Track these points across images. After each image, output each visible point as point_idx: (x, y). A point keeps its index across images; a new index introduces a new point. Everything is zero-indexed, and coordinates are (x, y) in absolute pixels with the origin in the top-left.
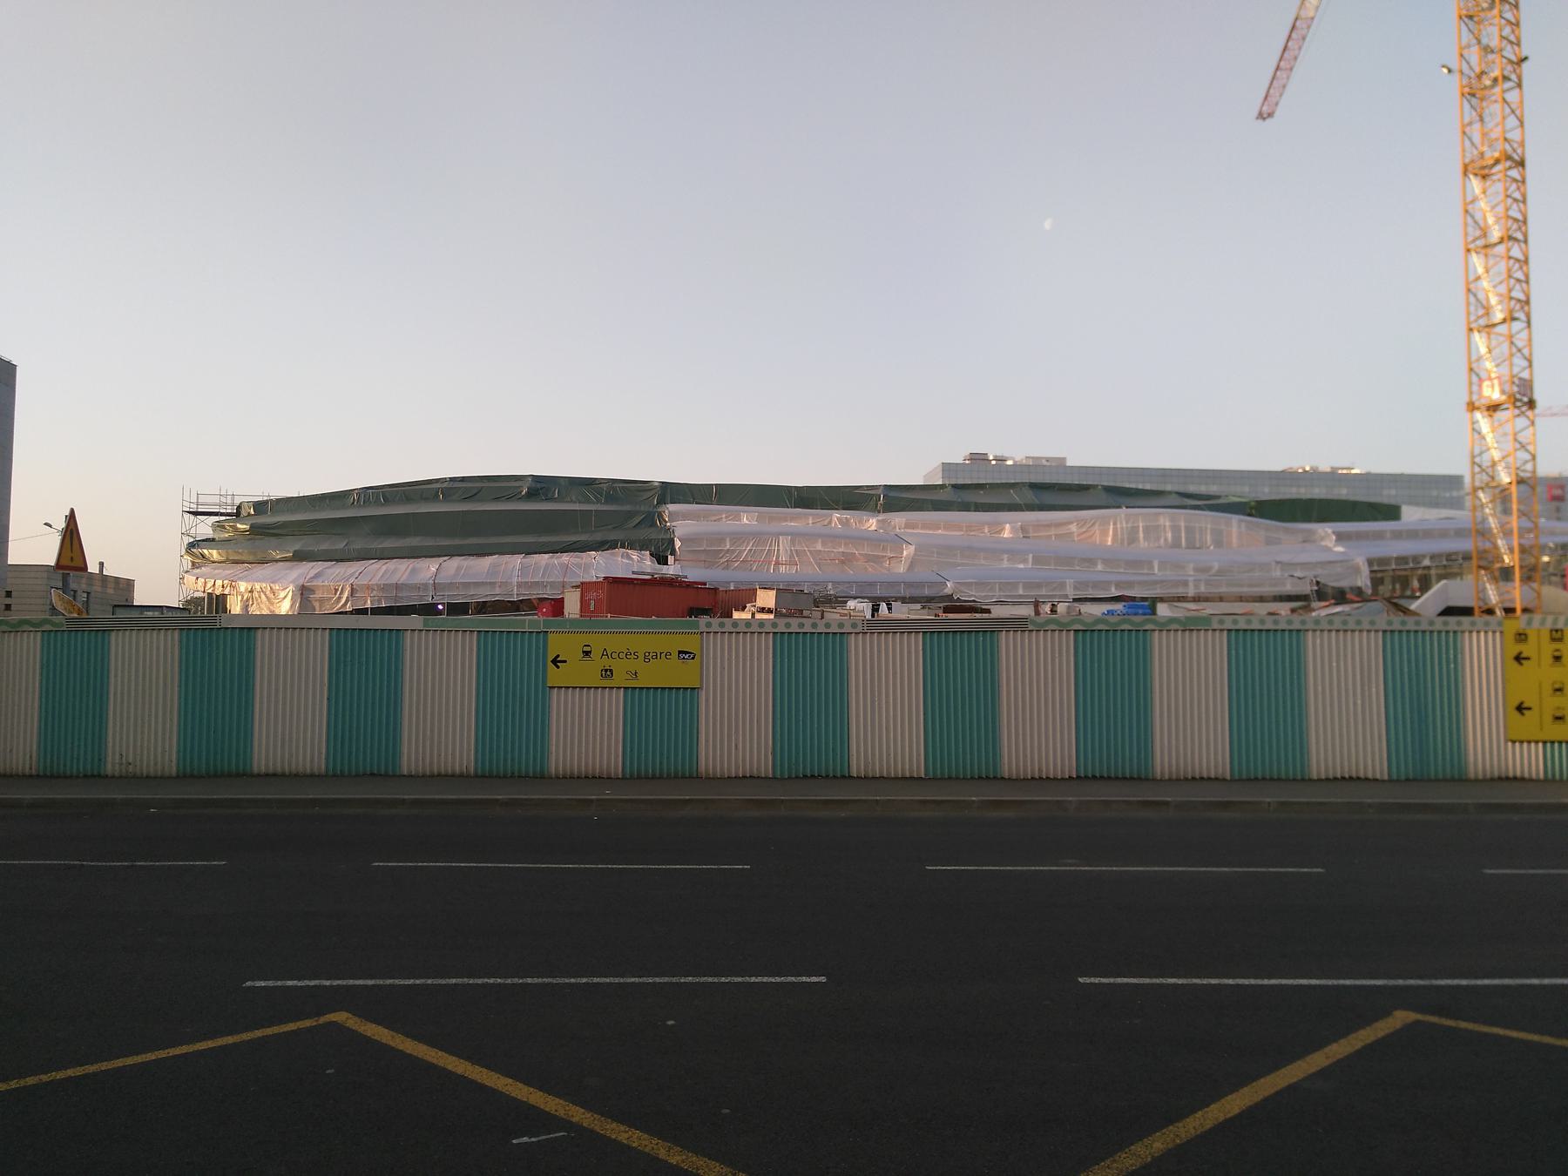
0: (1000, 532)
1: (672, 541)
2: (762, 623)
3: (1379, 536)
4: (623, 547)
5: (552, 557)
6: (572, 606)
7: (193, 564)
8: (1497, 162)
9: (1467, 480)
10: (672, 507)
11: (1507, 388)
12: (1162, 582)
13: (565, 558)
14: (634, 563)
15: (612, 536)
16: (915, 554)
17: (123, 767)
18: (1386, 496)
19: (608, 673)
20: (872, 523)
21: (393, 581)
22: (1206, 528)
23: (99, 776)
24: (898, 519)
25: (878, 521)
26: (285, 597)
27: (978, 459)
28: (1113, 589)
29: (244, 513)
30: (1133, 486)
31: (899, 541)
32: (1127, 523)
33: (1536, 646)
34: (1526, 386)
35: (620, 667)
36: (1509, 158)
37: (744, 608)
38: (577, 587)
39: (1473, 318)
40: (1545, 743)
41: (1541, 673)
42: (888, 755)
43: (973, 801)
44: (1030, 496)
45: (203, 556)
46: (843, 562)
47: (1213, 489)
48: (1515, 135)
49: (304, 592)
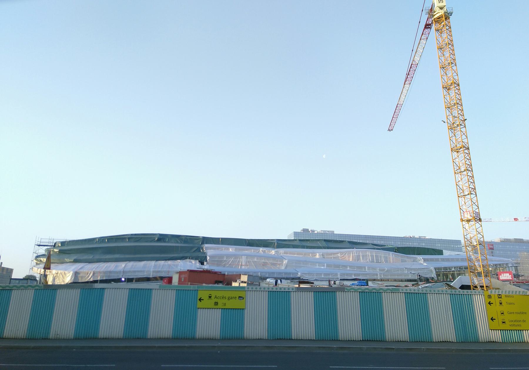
0: (315, 256)
1: (206, 257)
2: (244, 287)
3: (437, 260)
4: (189, 258)
5: (165, 262)
6: (175, 280)
7: (37, 264)
8: (461, 148)
9: (463, 242)
10: (206, 245)
11: (472, 214)
12: (369, 274)
13: (170, 262)
14: (194, 265)
15: (186, 255)
16: (288, 263)
17: (56, 335)
18: (438, 247)
19: (216, 304)
20: (273, 252)
21: (109, 270)
22: (382, 256)
23: (47, 339)
24: (282, 251)
25: (275, 251)
26: (70, 275)
27: (305, 231)
28: (353, 276)
29: (57, 245)
30: (356, 241)
31: (282, 258)
32: (356, 254)
33: (495, 300)
34: (478, 214)
35: (220, 302)
36: (464, 147)
37: (236, 281)
38: (177, 273)
39: (459, 193)
40: (501, 330)
41: (496, 309)
42: (304, 332)
43: (335, 347)
44: (324, 244)
45: (41, 261)
46: (263, 265)
47: (382, 243)
48: (465, 141)
49: (76, 274)
